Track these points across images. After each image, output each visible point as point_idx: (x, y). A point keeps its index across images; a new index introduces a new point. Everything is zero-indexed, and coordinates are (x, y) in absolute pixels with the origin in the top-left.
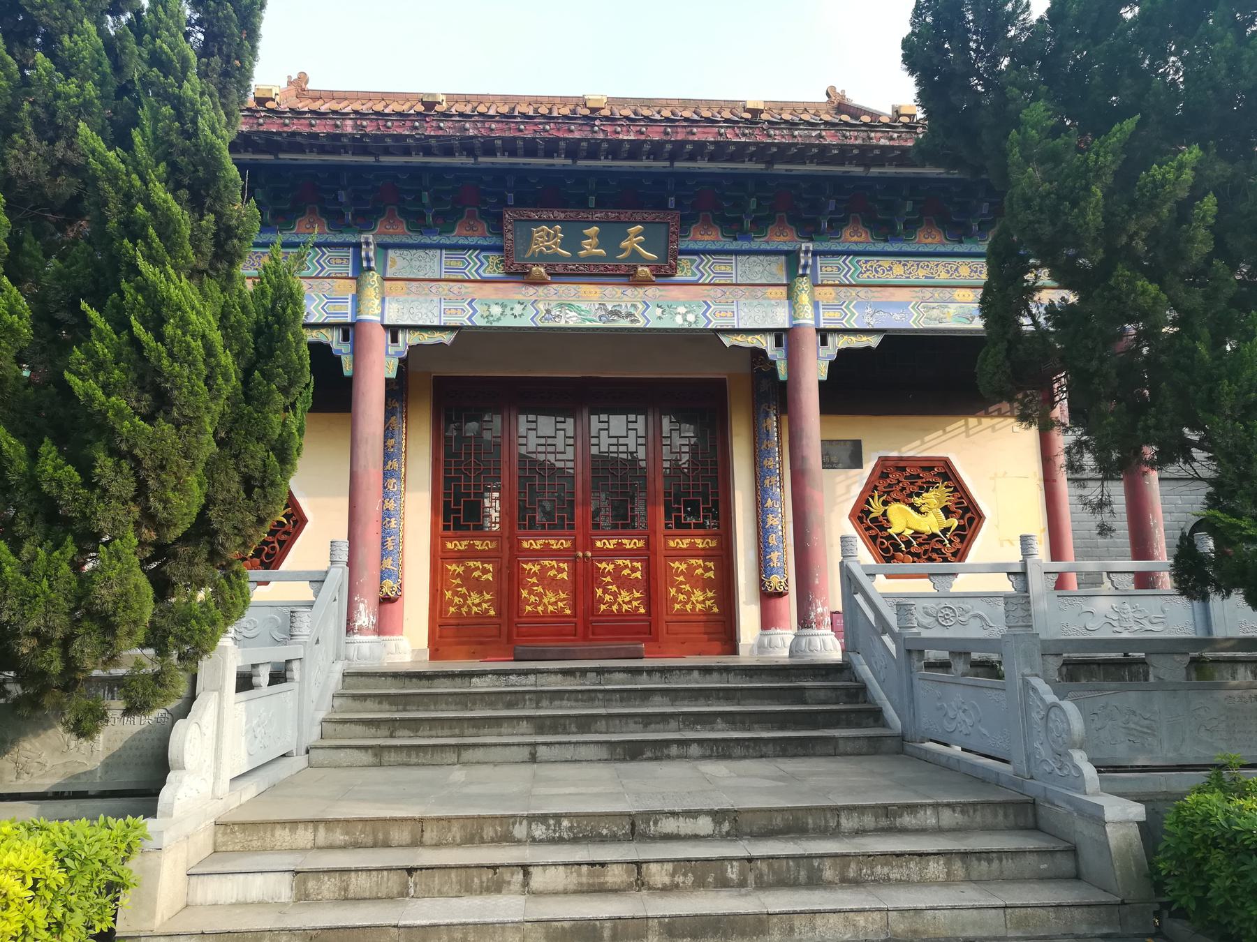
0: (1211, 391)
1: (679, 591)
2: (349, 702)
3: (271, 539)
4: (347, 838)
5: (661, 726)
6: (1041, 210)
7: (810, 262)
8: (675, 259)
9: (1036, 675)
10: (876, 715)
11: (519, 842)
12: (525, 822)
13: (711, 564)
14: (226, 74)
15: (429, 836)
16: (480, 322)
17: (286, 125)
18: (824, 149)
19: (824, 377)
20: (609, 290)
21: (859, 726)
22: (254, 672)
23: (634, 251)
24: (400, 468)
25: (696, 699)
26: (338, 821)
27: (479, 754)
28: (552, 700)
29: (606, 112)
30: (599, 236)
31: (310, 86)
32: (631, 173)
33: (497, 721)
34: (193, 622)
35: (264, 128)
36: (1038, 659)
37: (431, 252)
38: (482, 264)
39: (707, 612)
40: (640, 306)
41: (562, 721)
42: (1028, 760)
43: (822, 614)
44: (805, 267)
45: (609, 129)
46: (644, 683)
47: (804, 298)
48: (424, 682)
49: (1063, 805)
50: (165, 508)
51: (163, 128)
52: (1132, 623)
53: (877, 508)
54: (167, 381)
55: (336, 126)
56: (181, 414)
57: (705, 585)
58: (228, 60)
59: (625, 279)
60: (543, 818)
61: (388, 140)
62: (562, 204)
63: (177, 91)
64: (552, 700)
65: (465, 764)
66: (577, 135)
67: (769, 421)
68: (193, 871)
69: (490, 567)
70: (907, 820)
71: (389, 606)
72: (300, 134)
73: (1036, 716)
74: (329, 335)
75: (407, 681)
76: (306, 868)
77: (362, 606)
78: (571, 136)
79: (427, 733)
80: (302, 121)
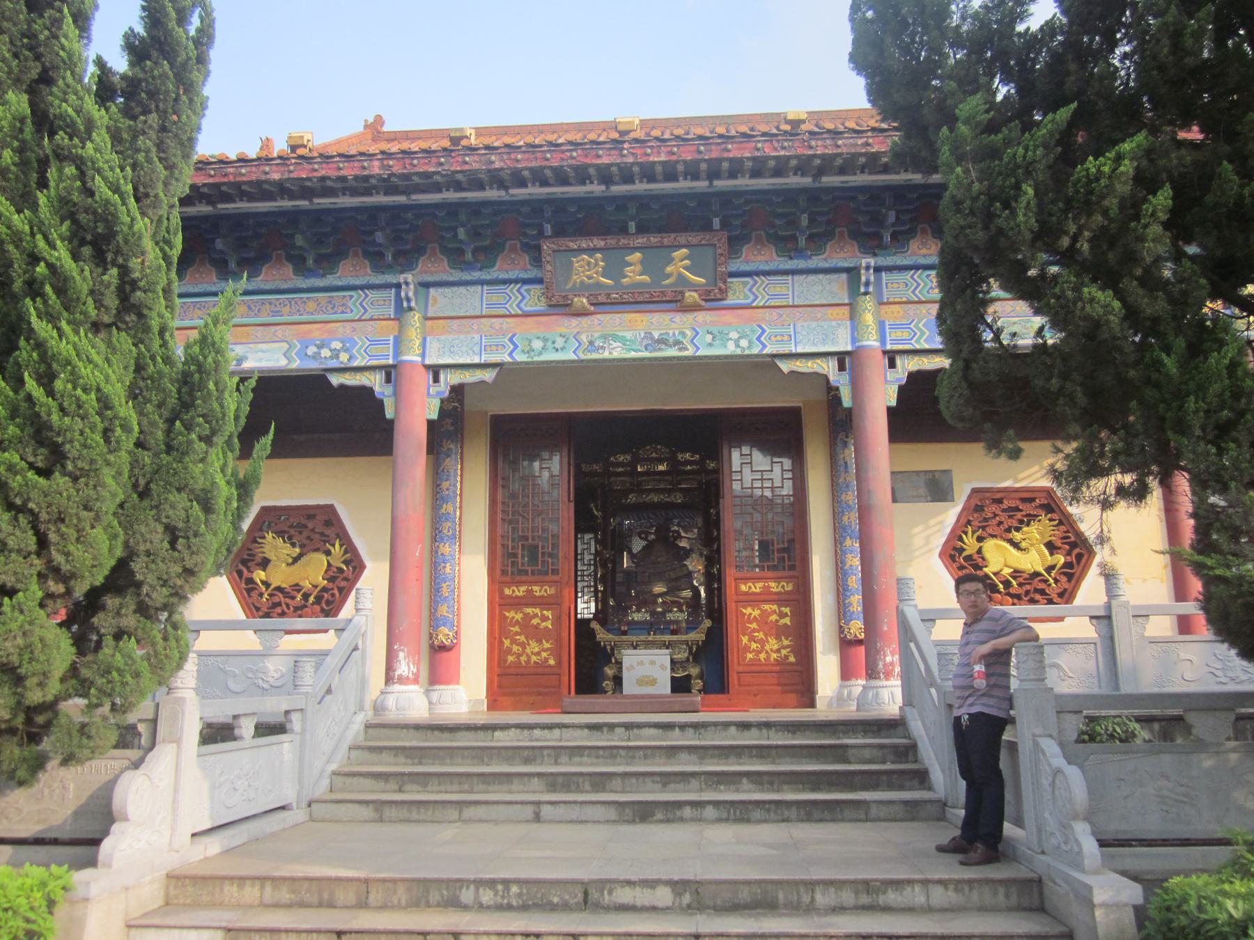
0: (1180, 407)
1: (752, 639)
2: (366, 753)
3: (331, 586)
4: (293, 896)
5: (681, 786)
6: (972, 213)
7: (872, 279)
8: (725, 282)
9: (1051, 736)
10: (922, 777)
11: (465, 908)
12: (472, 887)
13: (787, 610)
14: (163, 129)
15: (375, 897)
16: (520, 357)
17: (316, 170)
18: (874, 157)
19: (893, 403)
20: (656, 318)
21: (901, 788)
22: (236, 723)
23: (681, 276)
24: (455, 511)
25: (727, 757)
26: (284, 879)
27: (480, 811)
28: (571, 756)
29: (639, 134)
30: (642, 262)
31: (386, 129)
32: (672, 196)
33: (509, 776)
34: (115, 674)
35: (294, 175)
36: (1052, 716)
37: (472, 289)
38: (524, 297)
39: (782, 662)
40: (688, 333)
41: (575, 779)
42: (1039, 831)
43: (892, 664)
44: (867, 284)
45: (639, 152)
46: (676, 739)
47: (869, 318)
48: (446, 735)
49: (1063, 884)
50: (67, 561)
51: (65, 188)
52: (1239, 673)
53: (970, 544)
54: (59, 434)
55: (364, 168)
56: (76, 466)
57: (780, 632)
58: (163, 114)
59: (672, 306)
60: (492, 883)
61: (415, 178)
62: (604, 232)
63: (80, 151)
64: (571, 756)
65: (465, 821)
66: (606, 160)
67: (847, 451)
68: (133, 923)
69: (548, 614)
70: (891, 897)
71: (445, 655)
72: (329, 178)
73: (1046, 782)
74: (372, 378)
75: (429, 732)
76: (238, 925)
77: (401, 655)
78: (599, 161)
79: (436, 788)
80: (331, 165)
